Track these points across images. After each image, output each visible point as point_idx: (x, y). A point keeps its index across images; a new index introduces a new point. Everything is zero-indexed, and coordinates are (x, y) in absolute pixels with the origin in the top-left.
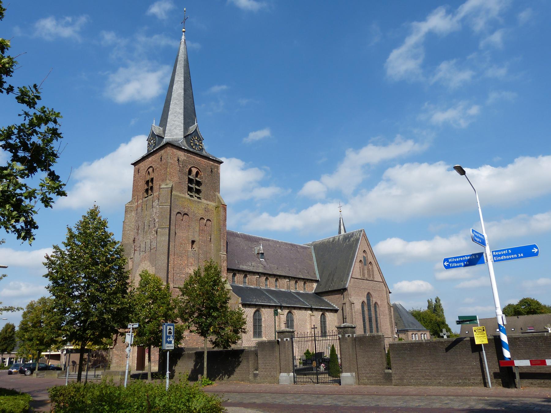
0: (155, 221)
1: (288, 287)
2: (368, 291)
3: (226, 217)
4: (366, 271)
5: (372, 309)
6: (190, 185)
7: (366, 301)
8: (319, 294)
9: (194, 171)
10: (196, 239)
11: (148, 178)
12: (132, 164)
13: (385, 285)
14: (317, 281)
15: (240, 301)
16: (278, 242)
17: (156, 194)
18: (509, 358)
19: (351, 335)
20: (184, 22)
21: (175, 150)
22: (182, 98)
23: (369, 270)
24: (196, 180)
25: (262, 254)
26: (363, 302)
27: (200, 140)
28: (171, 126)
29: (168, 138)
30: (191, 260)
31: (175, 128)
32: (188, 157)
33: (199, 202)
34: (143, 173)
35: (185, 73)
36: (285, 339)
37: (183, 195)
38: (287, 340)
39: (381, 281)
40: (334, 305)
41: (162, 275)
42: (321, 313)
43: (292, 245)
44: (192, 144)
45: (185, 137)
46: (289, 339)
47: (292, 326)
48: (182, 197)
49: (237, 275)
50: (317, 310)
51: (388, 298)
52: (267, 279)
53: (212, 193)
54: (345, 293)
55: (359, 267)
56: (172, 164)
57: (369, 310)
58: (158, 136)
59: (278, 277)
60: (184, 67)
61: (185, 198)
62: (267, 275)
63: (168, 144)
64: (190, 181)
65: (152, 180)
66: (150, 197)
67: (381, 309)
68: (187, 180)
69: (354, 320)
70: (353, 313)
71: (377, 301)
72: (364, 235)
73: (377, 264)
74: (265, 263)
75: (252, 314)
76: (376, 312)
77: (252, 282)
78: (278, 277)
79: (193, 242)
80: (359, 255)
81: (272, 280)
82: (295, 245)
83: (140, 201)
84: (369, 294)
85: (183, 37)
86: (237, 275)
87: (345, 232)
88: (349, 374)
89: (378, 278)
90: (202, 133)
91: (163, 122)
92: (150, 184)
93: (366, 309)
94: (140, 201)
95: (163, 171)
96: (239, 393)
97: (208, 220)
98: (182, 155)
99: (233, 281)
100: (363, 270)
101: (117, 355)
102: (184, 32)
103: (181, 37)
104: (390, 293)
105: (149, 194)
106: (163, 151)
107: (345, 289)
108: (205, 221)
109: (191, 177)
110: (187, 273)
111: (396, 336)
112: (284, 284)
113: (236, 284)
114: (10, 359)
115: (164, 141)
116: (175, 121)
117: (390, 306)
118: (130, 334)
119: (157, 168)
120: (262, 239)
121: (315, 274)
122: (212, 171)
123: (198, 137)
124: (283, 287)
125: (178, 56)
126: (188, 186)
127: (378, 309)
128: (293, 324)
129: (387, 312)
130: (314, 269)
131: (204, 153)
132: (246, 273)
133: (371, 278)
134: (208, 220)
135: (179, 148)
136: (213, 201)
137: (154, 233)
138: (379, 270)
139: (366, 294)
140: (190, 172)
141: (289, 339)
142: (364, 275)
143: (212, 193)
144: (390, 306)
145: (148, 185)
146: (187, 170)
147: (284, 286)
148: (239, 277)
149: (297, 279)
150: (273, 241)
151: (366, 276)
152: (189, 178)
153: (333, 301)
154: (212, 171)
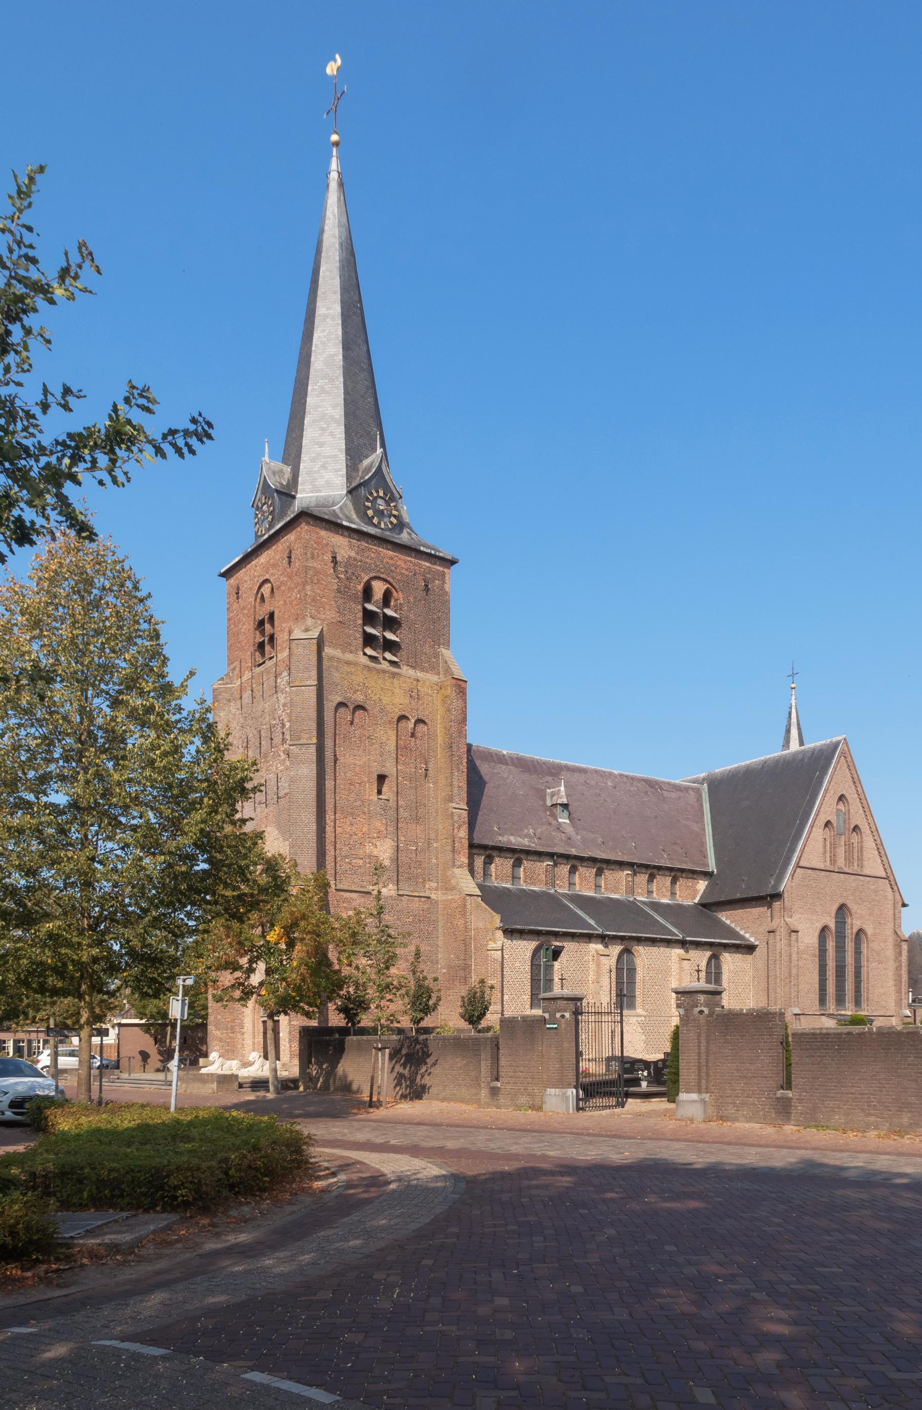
0: (283, 726)
1: (631, 890)
2: (841, 901)
3: (464, 713)
4: (841, 851)
5: (850, 946)
6: (369, 630)
7: (832, 925)
8: (708, 906)
9: (379, 588)
10: (390, 769)
11: (262, 613)
12: (223, 575)
13: (894, 886)
14: (707, 875)
15: (498, 923)
16: (611, 774)
17: (283, 655)
18: (80, 1061)
19: (706, 1011)
20: (333, 110)
21: (323, 533)
22: (339, 373)
23: (849, 846)
24: (385, 615)
25: (565, 806)
26: (824, 929)
27: (391, 497)
28: (313, 460)
29: (305, 496)
30: (378, 824)
31: (324, 467)
32: (361, 551)
33: (394, 675)
34: (249, 597)
35: (344, 290)
36: (558, 1015)
37: (349, 657)
38: (563, 1016)
39: (883, 874)
40: (747, 936)
41: (307, 864)
42: (708, 954)
43: (651, 784)
44: (370, 513)
45: (350, 492)
46: (567, 1015)
47: (718, 981)
48: (348, 663)
49: (497, 859)
50: (697, 945)
51: (896, 918)
52: (573, 870)
53: (427, 649)
54: (777, 905)
55: (821, 838)
56: (317, 572)
57: (840, 949)
58: (277, 491)
59: (601, 865)
60: (342, 268)
61: (356, 664)
62: (575, 861)
63: (305, 515)
64: (369, 617)
65: (272, 616)
66: (269, 663)
67: (875, 945)
68: (360, 615)
69: (794, 971)
70: (794, 956)
71: (865, 927)
72: (846, 755)
73: (875, 832)
74: (570, 830)
75: (529, 954)
76: (858, 952)
77: (533, 878)
78: (601, 865)
79: (381, 778)
80: (824, 806)
81: (587, 872)
82: (657, 782)
83: (247, 675)
84: (842, 908)
85: (334, 165)
86: (497, 859)
87: (801, 743)
88: (694, 1096)
89: (873, 866)
90: (395, 477)
91: (292, 452)
92: (267, 626)
93: (831, 945)
94: (247, 675)
95: (295, 594)
96: (508, 1129)
97: (419, 721)
98: (343, 546)
99: (486, 874)
100: (834, 846)
101: (221, 1040)
102: (336, 144)
103: (329, 163)
104: (904, 905)
105: (267, 656)
106: (291, 537)
107: (777, 896)
108: (411, 725)
109: (369, 607)
110: (370, 856)
111: (908, 1013)
112: (618, 882)
113: (494, 882)
114: (16, 1042)
115: (297, 506)
116: (321, 445)
117: (899, 940)
118: (180, 998)
119: (282, 583)
120: (568, 768)
121: (705, 857)
122: (427, 589)
123: (387, 490)
124: (616, 890)
125: (322, 231)
126: (364, 632)
127: (864, 947)
128: (634, 978)
129: (890, 952)
130: (703, 844)
131: (404, 537)
132: (519, 855)
133: (855, 868)
134: (419, 721)
135: (334, 526)
136: (434, 669)
137: (283, 756)
138: (880, 848)
139: (835, 907)
140: (367, 593)
141: (567, 1015)
142: (833, 861)
143: (427, 649)
144: (899, 940)
145: (263, 633)
146: (360, 588)
147: (616, 887)
148: (501, 866)
149: (653, 871)
150: (596, 772)
151: (841, 862)
152: (365, 609)
153: (743, 923)
154: (427, 589)
